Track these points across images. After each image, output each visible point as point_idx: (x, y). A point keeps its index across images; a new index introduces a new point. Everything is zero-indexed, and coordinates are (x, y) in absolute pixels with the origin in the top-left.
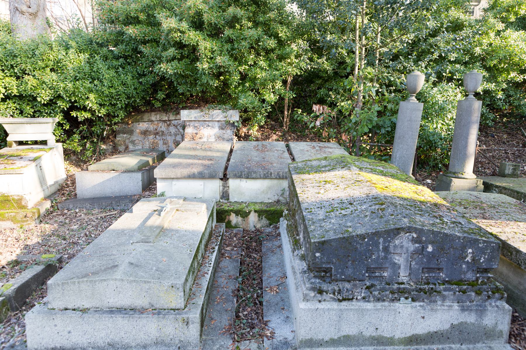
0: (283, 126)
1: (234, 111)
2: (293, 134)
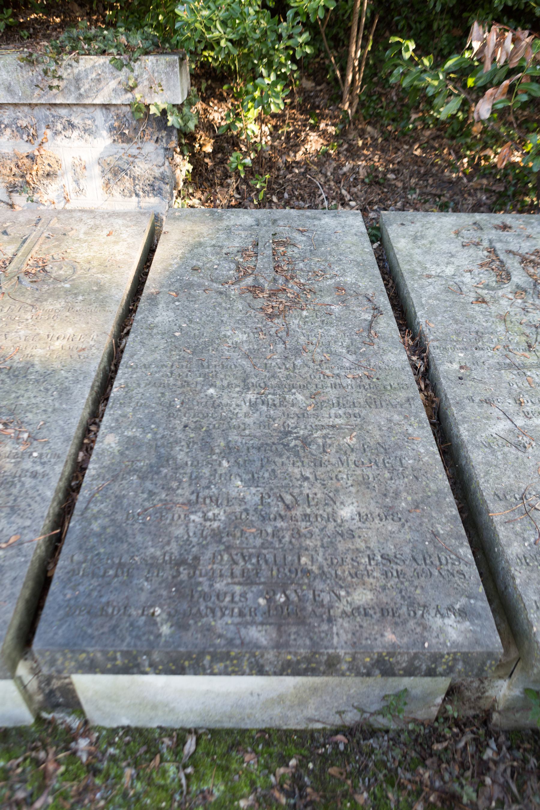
0: (340, 98)
1: (164, 59)
2: (369, 129)
